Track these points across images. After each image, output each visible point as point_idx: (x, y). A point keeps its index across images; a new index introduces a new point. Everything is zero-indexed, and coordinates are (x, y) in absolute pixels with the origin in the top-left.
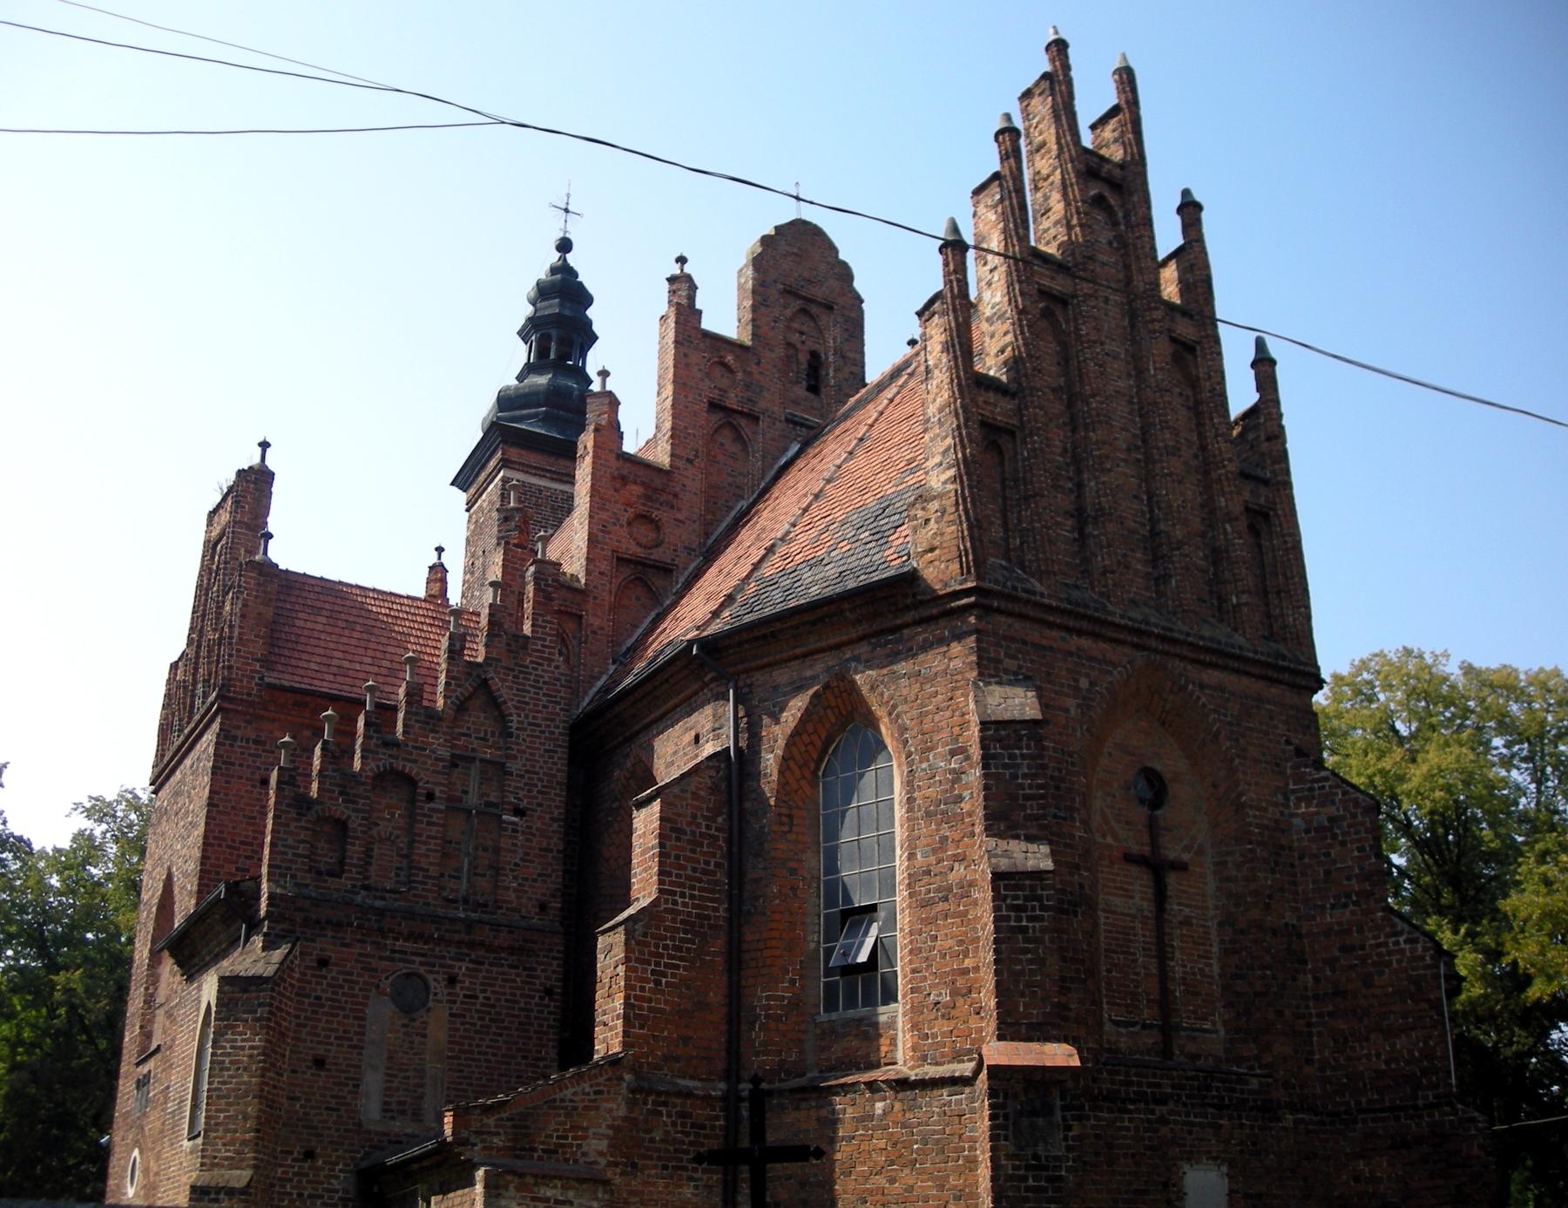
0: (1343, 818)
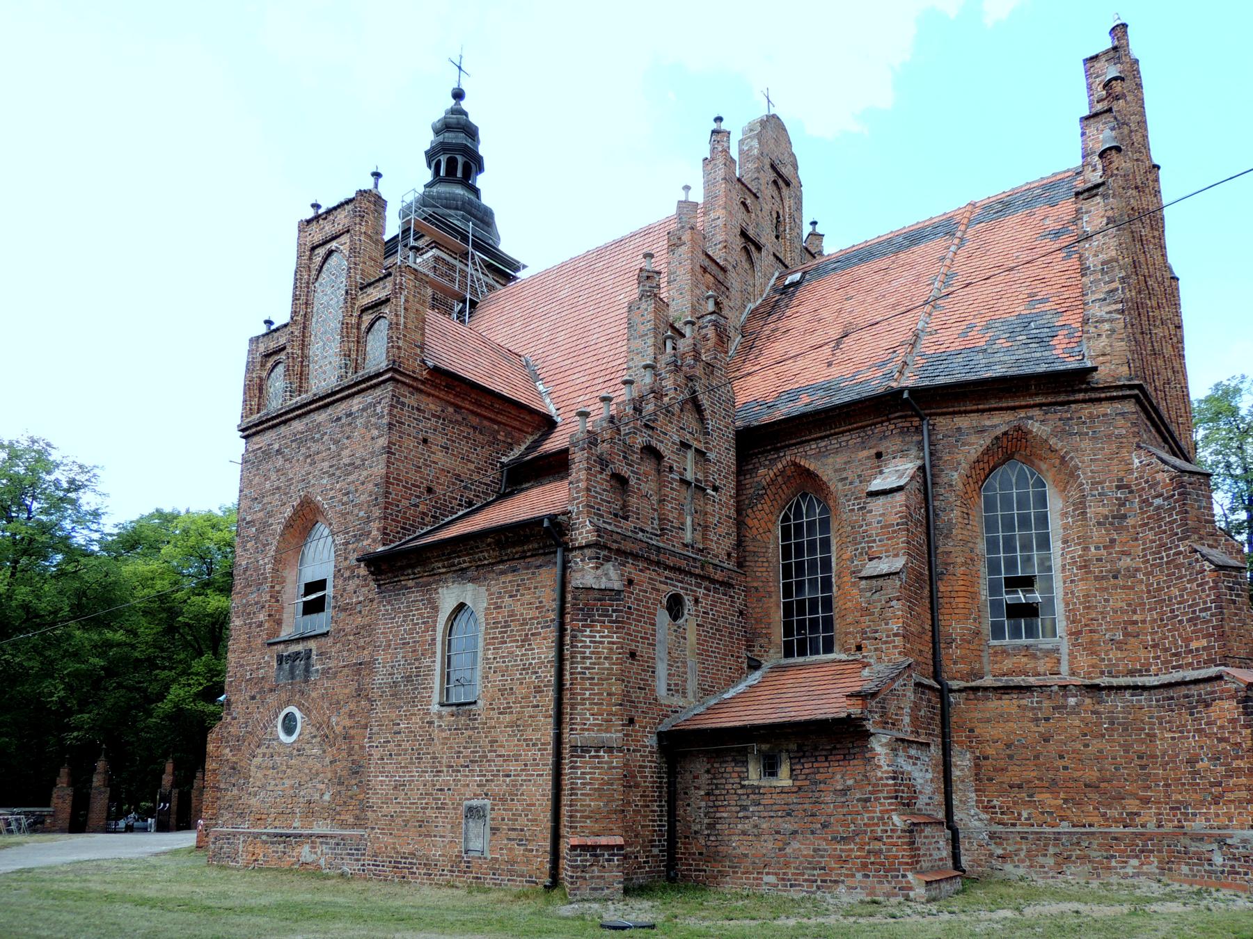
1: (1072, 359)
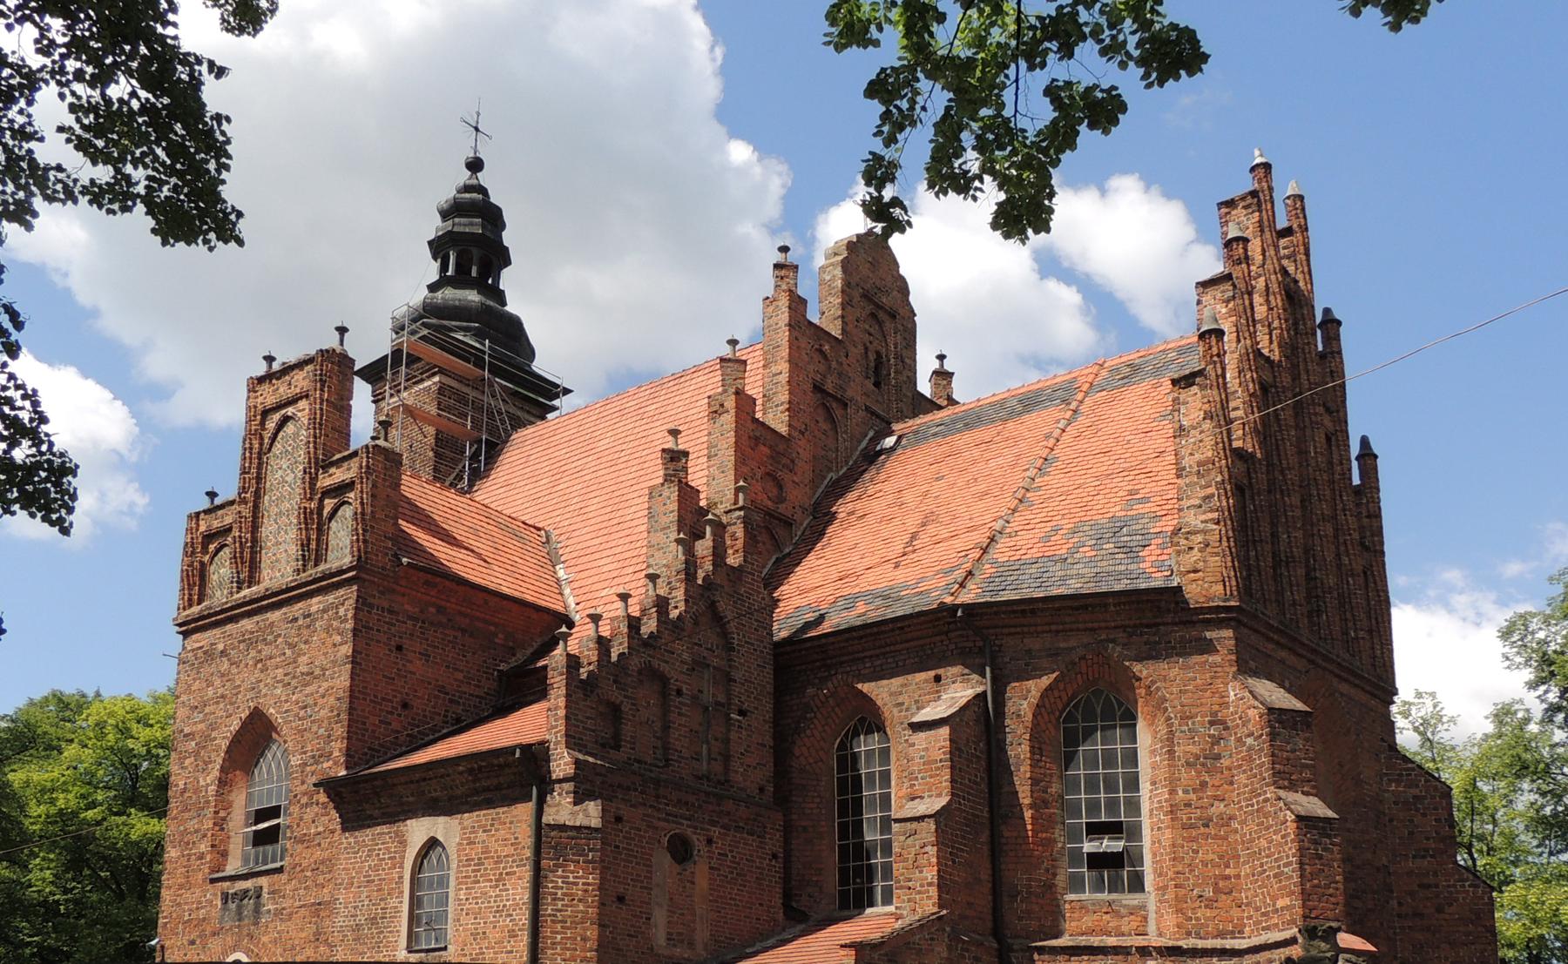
0: (1425, 797)
1: (1160, 574)
